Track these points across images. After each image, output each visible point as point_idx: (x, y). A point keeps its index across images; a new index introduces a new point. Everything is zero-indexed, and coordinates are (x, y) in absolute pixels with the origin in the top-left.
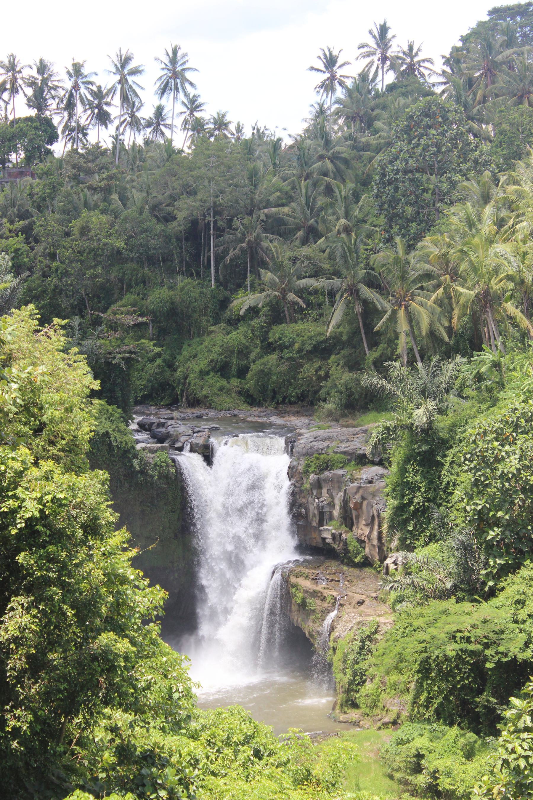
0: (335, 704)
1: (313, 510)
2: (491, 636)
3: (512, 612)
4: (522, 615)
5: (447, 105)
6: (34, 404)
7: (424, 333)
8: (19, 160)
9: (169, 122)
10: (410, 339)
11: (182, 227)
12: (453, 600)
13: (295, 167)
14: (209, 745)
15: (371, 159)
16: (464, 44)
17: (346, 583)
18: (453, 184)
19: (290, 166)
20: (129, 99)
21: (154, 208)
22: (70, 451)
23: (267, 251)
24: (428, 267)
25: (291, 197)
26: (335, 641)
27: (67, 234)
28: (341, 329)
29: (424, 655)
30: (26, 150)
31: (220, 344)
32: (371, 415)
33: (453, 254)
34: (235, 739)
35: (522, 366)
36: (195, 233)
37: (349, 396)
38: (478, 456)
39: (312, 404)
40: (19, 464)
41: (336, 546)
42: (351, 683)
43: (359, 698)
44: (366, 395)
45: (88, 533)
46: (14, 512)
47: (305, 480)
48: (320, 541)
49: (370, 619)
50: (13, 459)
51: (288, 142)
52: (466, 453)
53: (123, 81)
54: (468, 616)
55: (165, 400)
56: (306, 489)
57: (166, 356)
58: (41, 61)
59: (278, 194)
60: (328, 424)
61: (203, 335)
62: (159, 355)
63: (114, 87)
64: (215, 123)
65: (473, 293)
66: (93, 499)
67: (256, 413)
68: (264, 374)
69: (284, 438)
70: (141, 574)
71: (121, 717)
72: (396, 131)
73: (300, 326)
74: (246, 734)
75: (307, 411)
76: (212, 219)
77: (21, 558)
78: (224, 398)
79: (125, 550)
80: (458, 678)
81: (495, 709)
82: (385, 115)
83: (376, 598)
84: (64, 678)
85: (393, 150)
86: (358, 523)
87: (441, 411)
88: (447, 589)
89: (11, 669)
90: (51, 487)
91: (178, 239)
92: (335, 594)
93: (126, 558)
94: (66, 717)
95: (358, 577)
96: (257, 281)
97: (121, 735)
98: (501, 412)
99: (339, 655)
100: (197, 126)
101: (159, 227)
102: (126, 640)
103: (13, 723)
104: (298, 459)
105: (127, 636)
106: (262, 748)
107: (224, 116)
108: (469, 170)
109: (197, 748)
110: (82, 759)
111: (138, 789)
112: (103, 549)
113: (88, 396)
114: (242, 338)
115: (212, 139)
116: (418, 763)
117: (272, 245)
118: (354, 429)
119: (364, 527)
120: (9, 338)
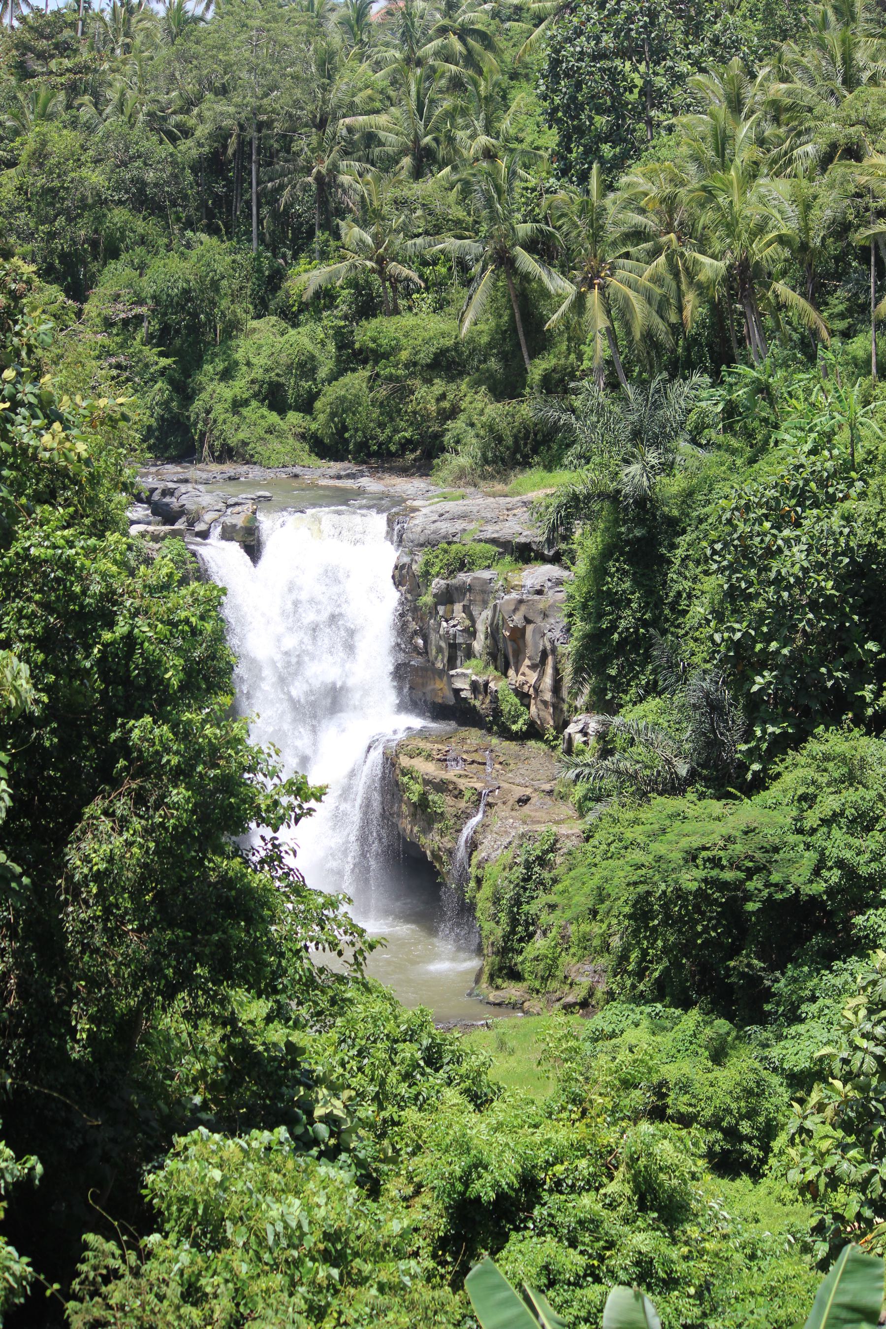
0: (480, 972)
2: (758, 855)
3: (795, 813)
4: (812, 819)
17: (498, 766)
24: (639, 219)
29: (641, 889)
35: (808, 391)
38: (736, 547)
41: (477, 703)
42: (507, 938)
43: (522, 963)
48: (450, 696)
49: (541, 828)
52: (714, 542)
54: (712, 822)
56: (425, 605)
59: (369, 92)
60: (462, 491)
65: (721, 266)
67: (332, 472)
68: (344, 407)
69: (385, 515)
80: (699, 928)
81: (761, 978)
83: (550, 792)
92: (478, 785)
95: (517, 757)
96: (333, 243)
98: (773, 470)
99: (486, 890)
104: (411, 553)
114: (306, 341)
118: (508, 499)
119: (527, 671)
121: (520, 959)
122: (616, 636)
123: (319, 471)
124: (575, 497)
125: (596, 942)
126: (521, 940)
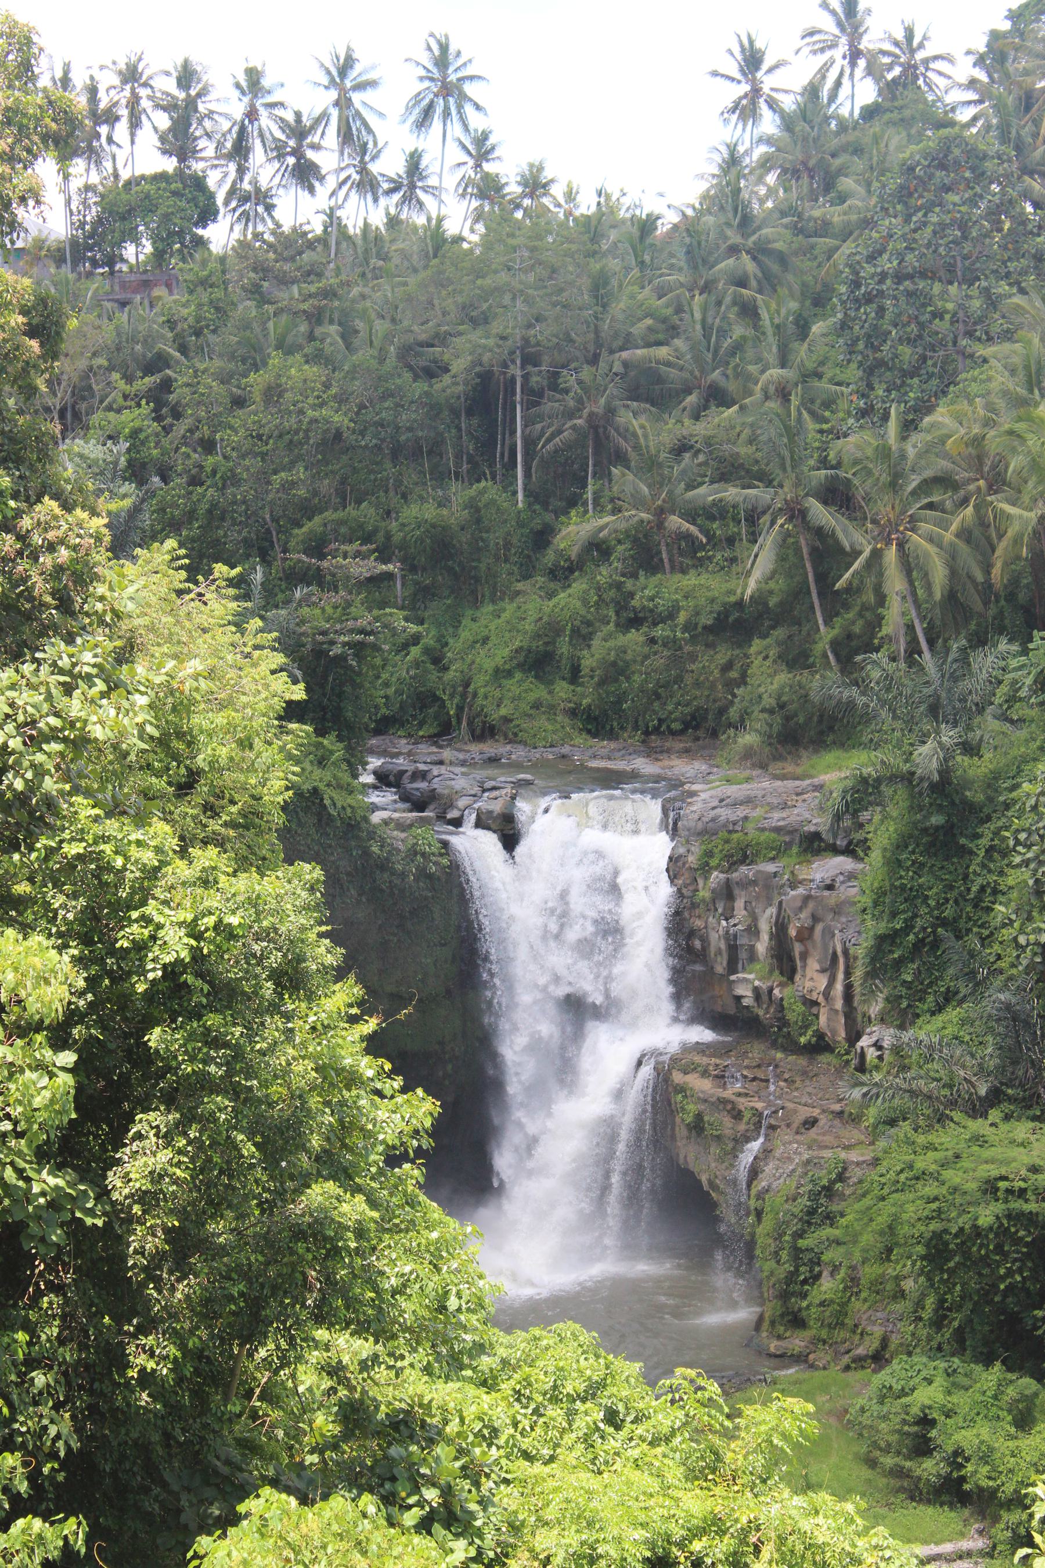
0: (761, 1319)
1: (716, 941)
5: (982, 147)
6: (180, 735)
7: (938, 596)
8: (142, 257)
9: (433, 181)
10: (910, 605)
11: (461, 388)
12: (995, 1115)
13: (680, 269)
14: (518, 1400)
15: (830, 253)
16: (1014, 24)
18: (992, 302)
19: (672, 267)
20: (354, 137)
21: (406, 352)
22: (246, 827)
23: (626, 433)
25: (674, 328)
26: (759, 1196)
27: (239, 402)
28: (772, 585)
29: (934, 1226)
30: (155, 239)
31: (536, 616)
32: (830, 757)
33: (994, 441)
34: (569, 1389)
36: (487, 397)
37: (787, 719)
39: (714, 734)
40: (150, 854)
41: (761, 1013)
43: (808, 1307)
44: (821, 716)
45: (284, 988)
46: (140, 947)
47: (701, 882)
49: (827, 1154)
50: (139, 843)
51: (670, 219)
52: (1018, 831)
53: (343, 103)
55: (425, 727)
56: (703, 900)
57: (429, 640)
58: (186, 64)
59: (649, 322)
60: (747, 773)
61: (502, 599)
62: (416, 639)
63: (324, 116)
64: (524, 183)
66: (294, 922)
67: (603, 752)
70: (388, 1066)
71: (350, 1347)
72: (880, 196)
73: (690, 580)
74: (589, 1378)
75: (704, 748)
76: (519, 373)
77: (154, 1038)
78: (542, 722)
79: (353, 1020)
80: (1002, 1271)
82: (859, 164)
83: (841, 1113)
84: (244, 1273)
85: (875, 235)
86: (804, 967)
87: (970, 749)
88: (979, 1098)
89: (136, 1252)
90: (213, 900)
91: (455, 413)
92: (759, 1105)
93: (357, 1037)
94: (241, 1346)
95: (805, 1073)
97: (348, 1379)
100: (488, 188)
101: (421, 387)
102: (360, 1198)
103: (141, 1360)
104: (688, 842)
105: (358, 1189)
106: (621, 1407)
107: (541, 169)
108: (1024, 272)
109: (494, 1405)
110: (273, 1426)
111: (382, 1485)
112: (312, 1019)
113: (280, 718)
114: (578, 604)
115: (519, 215)
116: (924, 1436)
117: (634, 420)
118: (797, 783)
119: (816, 975)
120: (131, 606)
121: (804, 1304)
122: (911, 937)
123: (590, 752)
124: (864, 780)
125: (890, 1286)
126: (805, 1282)
